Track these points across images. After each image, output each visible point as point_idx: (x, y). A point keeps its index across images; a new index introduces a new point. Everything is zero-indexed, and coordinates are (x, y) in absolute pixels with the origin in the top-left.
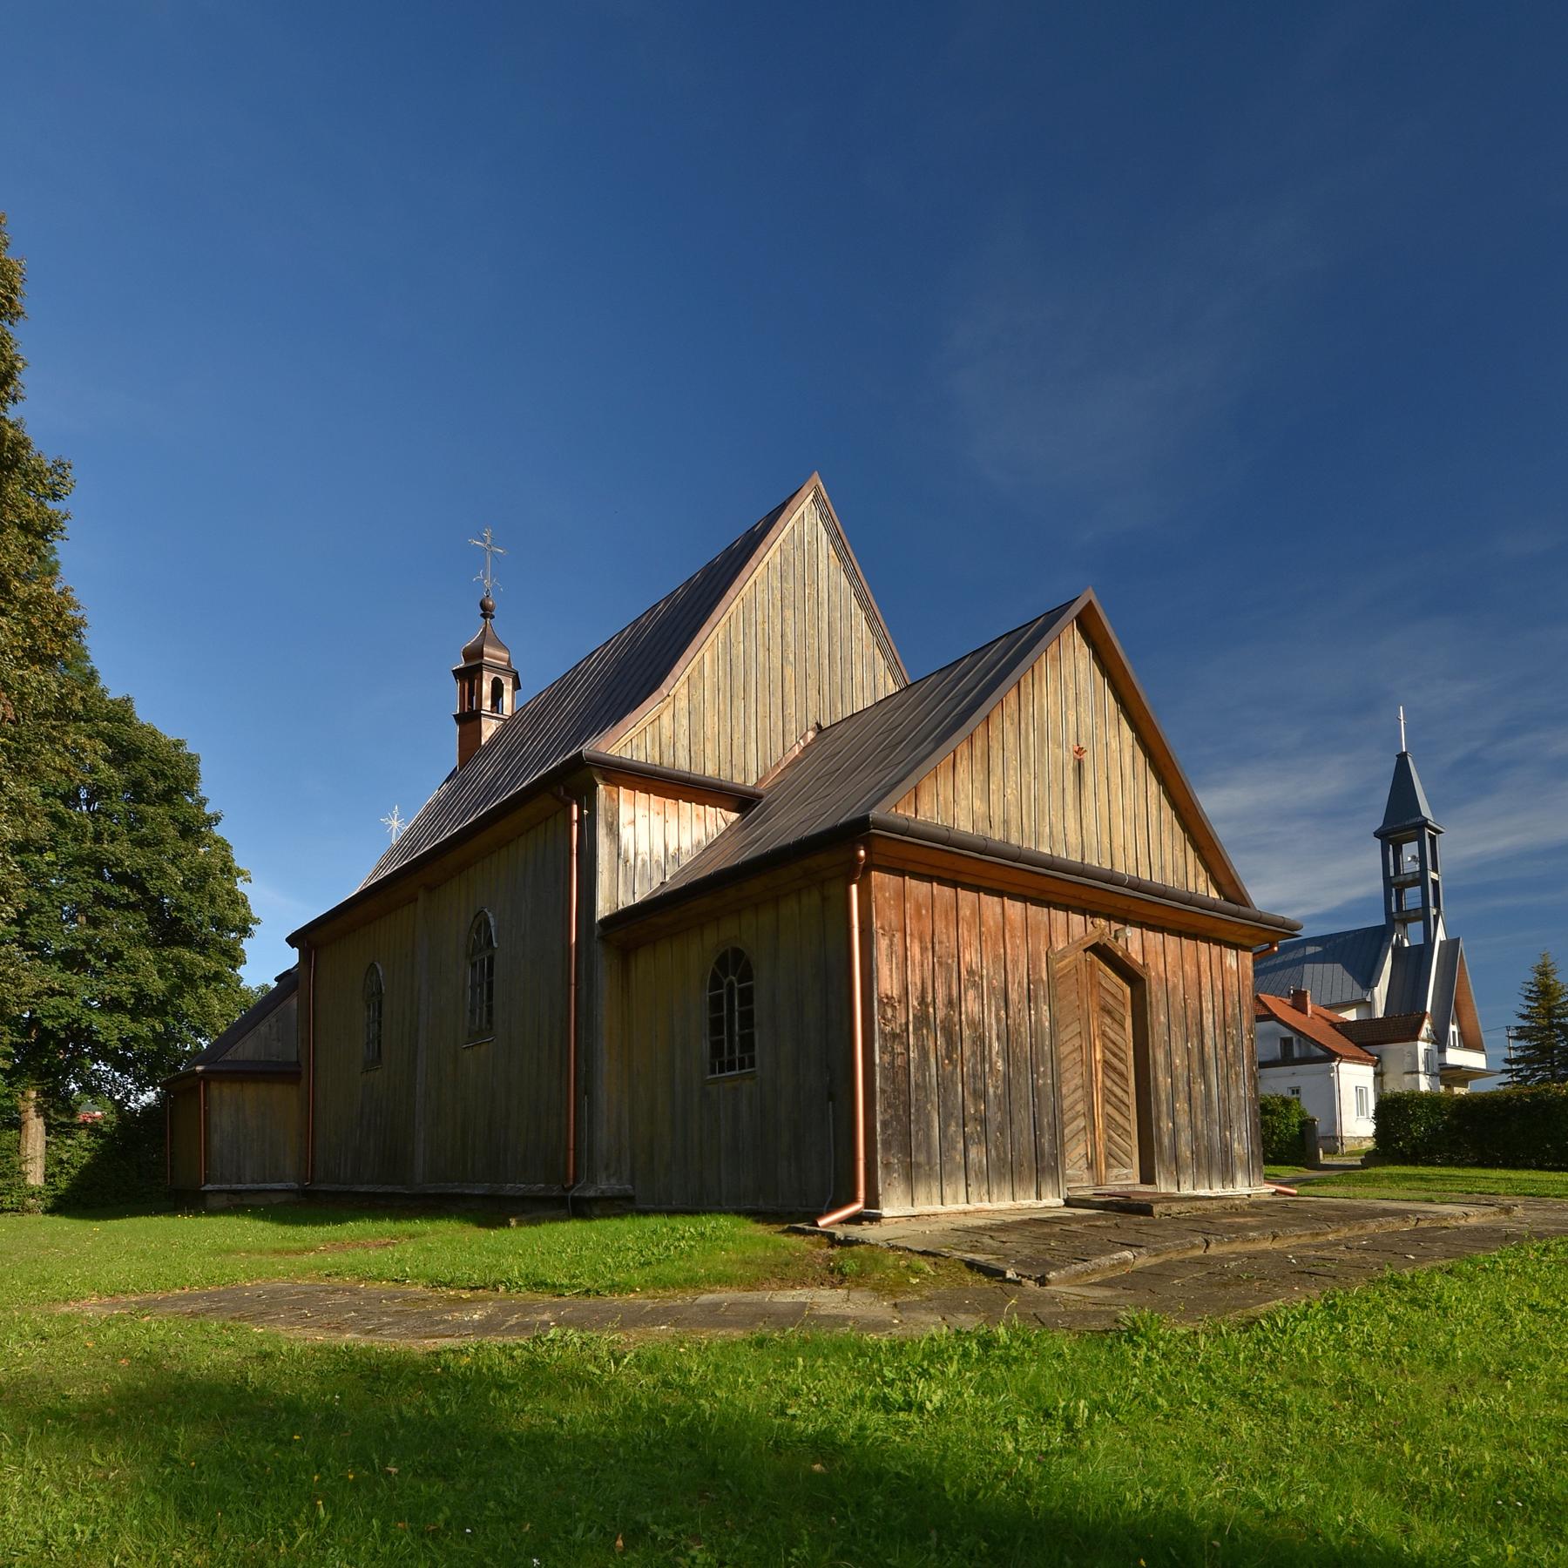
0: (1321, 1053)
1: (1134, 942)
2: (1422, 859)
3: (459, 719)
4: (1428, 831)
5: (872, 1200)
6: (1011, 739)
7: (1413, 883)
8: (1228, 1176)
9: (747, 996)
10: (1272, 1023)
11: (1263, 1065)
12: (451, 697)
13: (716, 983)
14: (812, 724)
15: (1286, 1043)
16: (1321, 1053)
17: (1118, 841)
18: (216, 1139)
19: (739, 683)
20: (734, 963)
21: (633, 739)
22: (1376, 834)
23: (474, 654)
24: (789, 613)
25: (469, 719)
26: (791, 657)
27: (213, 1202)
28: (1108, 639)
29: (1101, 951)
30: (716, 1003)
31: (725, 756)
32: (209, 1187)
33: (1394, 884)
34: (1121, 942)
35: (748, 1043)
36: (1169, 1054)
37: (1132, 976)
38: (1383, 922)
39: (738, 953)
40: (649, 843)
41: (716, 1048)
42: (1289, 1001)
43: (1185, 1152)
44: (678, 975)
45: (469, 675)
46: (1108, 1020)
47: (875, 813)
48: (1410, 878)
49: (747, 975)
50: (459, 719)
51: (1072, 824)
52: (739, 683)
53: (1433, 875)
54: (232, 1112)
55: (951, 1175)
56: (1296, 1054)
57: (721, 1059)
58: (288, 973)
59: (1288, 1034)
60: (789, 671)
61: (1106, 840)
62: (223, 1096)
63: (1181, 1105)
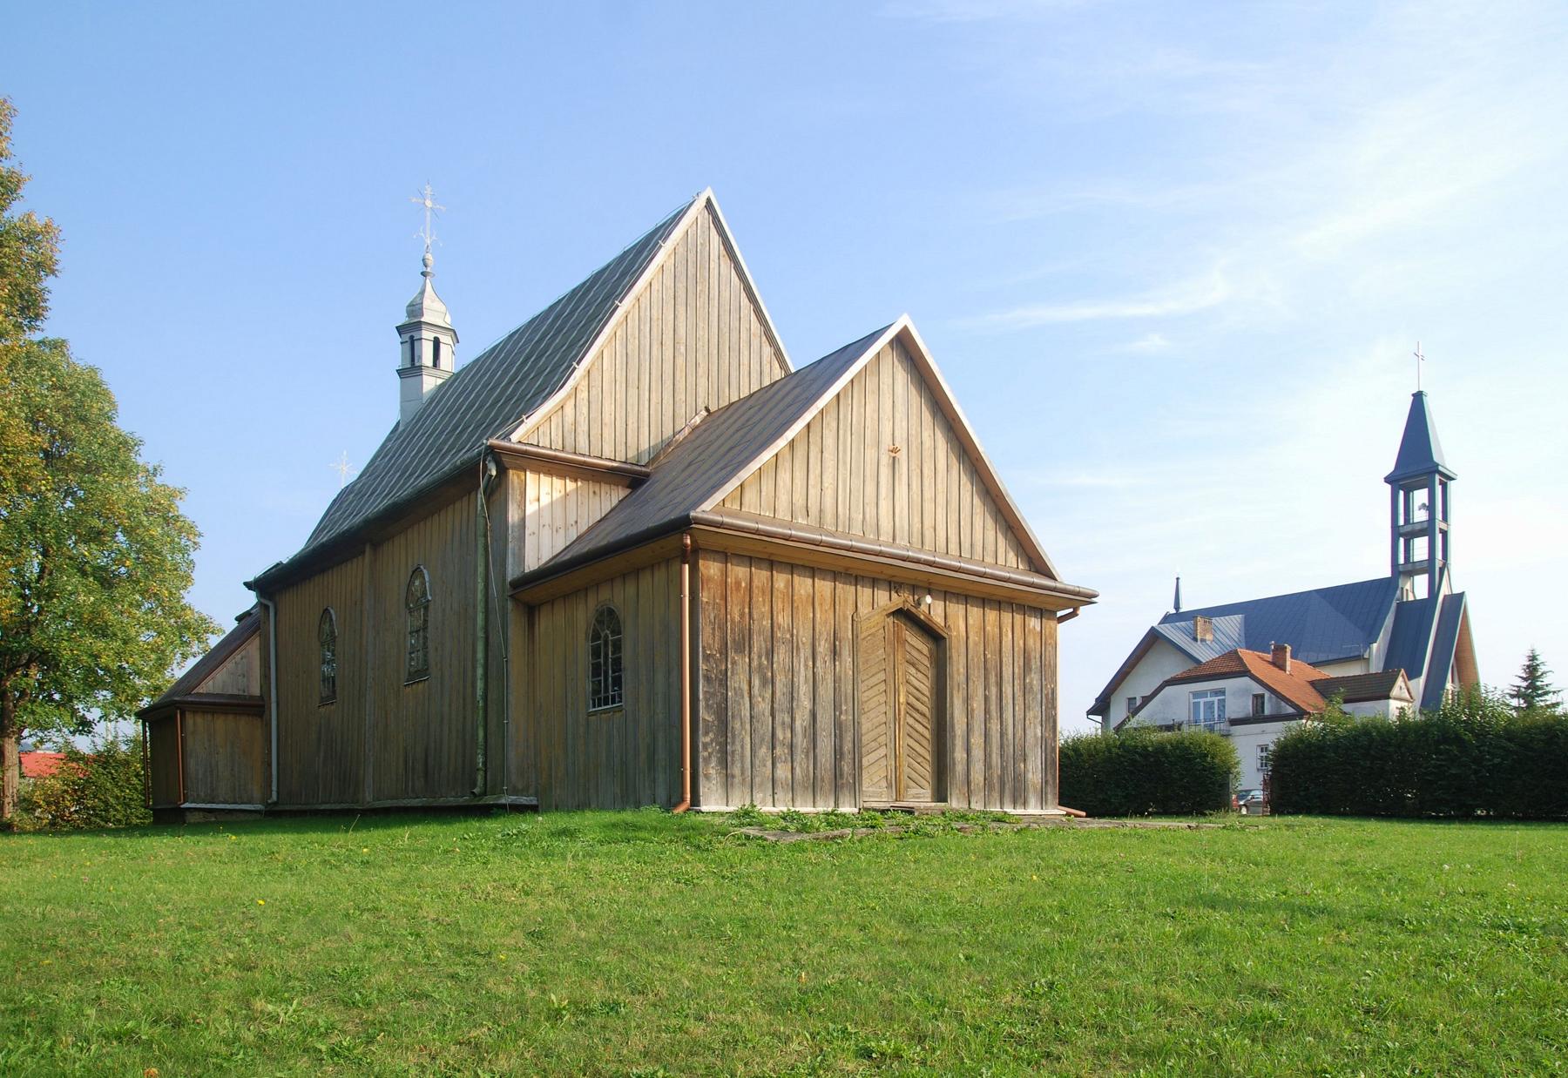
0: (1291, 710)
1: (933, 608)
2: (1430, 508)
3: (401, 373)
4: (1437, 477)
5: (695, 801)
6: (829, 441)
7: (1420, 533)
8: (1019, 798)
9: (617, 647)
10: (1246, 680)
11: (1234, 722)
12: (395, 354)
13: (596, 637)
14: (701, 406)
15: (1259, 699)
16: (1291, 710)
17: (928, 523)
18: (192, 763)
19: (633, 375)
20: (608, 618)
21: (528, 432)
22: (1388, 480)
23: (415, 309)
24: (681, 309)
25: (411, 370)
26: (683, 349)
27: (191, 818)
28: (922, 357)
29: (902, 614)
30: (596, 653)
31: (621, 439)
32: (187, 805)
33: (1403, 533)
34: (924, 608)
35: (618, 682)
36: (967, 700)
37: (934, 635)
38: (1385, 572)
39: (611, 612)
40: (547, 516)
41: (596, 692)
42: (1269, 657)
43: (978, 776)
44: (567, 627)
45: (410, 331)
46: (913, 671)
47: (692, 514)
48: (1418, 527)
49: (617, 631)
50: (401, 373)
51: (885, 506)
52: (633, 375)
53: (1443, 526)
54: (203, 739)
55: (761, 785)
56: (1267, 712)
57: (600, 697)
58: (247, 614)
59: (1259, 690)
60: (680, 361)
61: (917, 520)
62: (196, 725)
63: (977, 740)
